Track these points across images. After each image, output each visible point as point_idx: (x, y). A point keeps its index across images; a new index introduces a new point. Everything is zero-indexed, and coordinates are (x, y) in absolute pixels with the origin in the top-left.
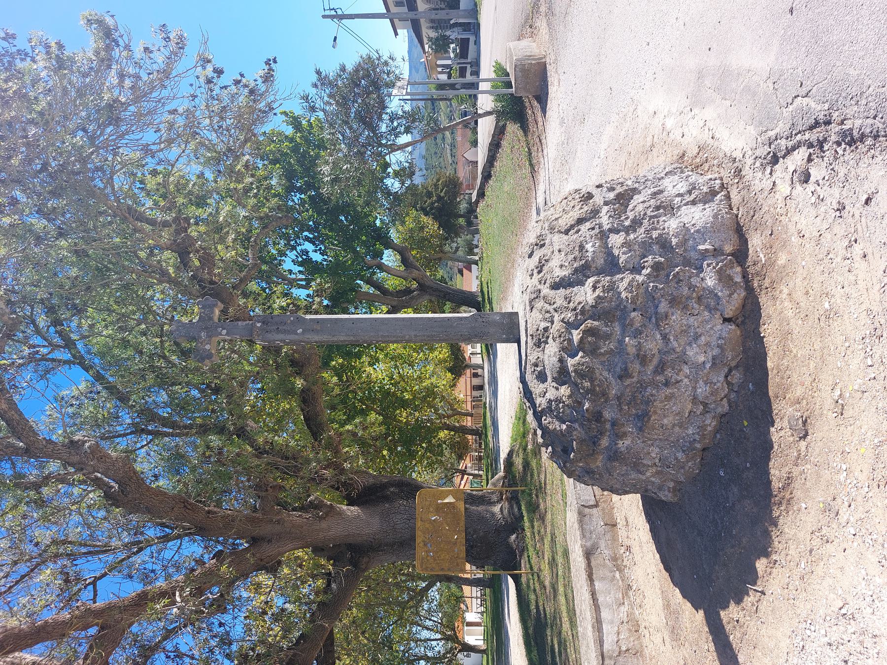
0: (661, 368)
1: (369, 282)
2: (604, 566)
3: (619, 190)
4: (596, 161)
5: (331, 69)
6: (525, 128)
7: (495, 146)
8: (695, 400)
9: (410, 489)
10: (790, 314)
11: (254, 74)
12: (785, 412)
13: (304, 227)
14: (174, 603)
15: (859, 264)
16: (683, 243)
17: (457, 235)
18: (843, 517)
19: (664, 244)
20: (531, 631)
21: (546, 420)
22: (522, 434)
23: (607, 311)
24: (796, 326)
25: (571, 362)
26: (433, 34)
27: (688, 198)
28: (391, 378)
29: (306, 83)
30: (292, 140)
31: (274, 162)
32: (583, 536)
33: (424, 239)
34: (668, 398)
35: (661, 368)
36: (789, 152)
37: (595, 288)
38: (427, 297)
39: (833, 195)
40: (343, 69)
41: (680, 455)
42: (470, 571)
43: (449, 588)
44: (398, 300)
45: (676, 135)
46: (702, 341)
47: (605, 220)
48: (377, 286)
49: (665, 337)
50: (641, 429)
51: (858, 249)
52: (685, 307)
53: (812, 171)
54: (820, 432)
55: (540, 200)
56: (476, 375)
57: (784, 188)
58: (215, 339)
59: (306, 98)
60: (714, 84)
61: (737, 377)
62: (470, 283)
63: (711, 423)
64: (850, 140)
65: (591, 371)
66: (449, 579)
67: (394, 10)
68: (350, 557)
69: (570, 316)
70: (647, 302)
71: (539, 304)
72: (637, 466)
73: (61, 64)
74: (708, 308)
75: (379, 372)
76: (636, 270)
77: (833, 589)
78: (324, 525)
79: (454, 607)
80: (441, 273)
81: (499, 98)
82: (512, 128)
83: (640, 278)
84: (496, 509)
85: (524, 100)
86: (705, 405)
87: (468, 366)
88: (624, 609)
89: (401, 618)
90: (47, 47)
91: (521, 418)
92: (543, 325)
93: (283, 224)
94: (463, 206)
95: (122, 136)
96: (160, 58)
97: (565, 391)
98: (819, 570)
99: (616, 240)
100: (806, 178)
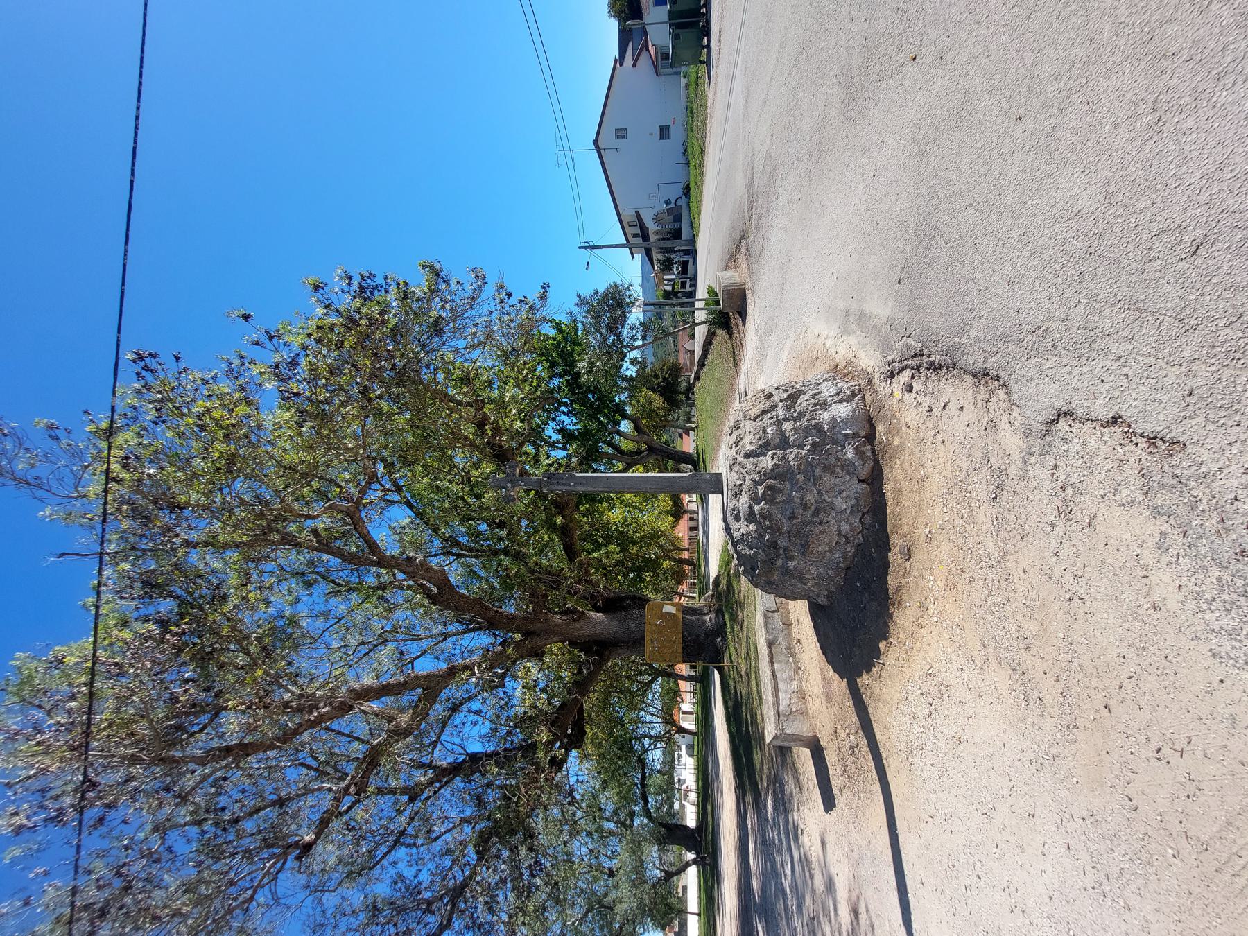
0: (817, 512)
1: (610, 444)
2: (782, 653)
3: (791, 391)
4: (780, 364)
5: (587, 292)
6: (730, 333)
7: (708, 343)
8: (839, 534)
9: (642, 602)
10: (901, 477)
11: (533, 295)
12: (897, 542)
13: (561, 404)
14: (474, 674)
15: (940, 447)
16: (832, 429)
17: (678, 407)
18: (931, 610)
19: (819, 429)
20: (730, 704)
21: (739, 548)
22: (725, 564)
23: (780, 474)
24: (905, 487)
25: (756, 508)
26: (661, 257)
27: (837, 398)
28: (625, 520)
29: (570, 303)
30: (554, 339)
31: (542, 355)
32: (767, 632)
33: (652, 411)
34: (821, 533)
35: (817, 512)
36: (901, 371)
37: (773, 458)
38: (654, 457)
39: (926, 401)
40: (596, 293)
41: (830, 572)
42: (683, 669)
43: (668, 683)
44: (631, 459)
45: (832, 352)
46: (845, 495)
47: (780, 413)
48: (616, 447)
49: (819, 492)
50: (803, 554)
51: (939, 437)
52: (833, 472)
53: (914, 385)
54: (919, 556)
55: (742, 387)
56: (692, 519)
57: (898, 395)
58: (517, 489)
59: (570, 313)
60: (853, 320)
61: (868, 519)
62: (688, 445)
63: (851, 550)
64: (934, 367)
65: (770, 514)
66: (669, 675)
67: (632, 240)
68: (598, 649)
69: (756, 476)
70: (807, 467)
71: (737, 468)
72: (802, 579)
73: (405, 296)
74: (848, 473)
75: (616, 515)
76: (801, 447)
77: (924, 659)
78: (578, 625)
79: (673, 696)
80: (665, 437)
81: (711, 313)
82: (721, 333)
83: (803, 452)
84: (707, 618)
85: (730, 312)
86: (847, 538)
87: (686, 512)
88: (795, 683)
89: (631, 703)
90: (398, 284)
91: (725, 550)
92: (739, 482)
93: (545, 402)
94: (683, 385)
95: (444, 344)
96: (469, 289)
97: (752, 527)
98: (917, 646)
99: (787, 426)
100: (910, 389)
